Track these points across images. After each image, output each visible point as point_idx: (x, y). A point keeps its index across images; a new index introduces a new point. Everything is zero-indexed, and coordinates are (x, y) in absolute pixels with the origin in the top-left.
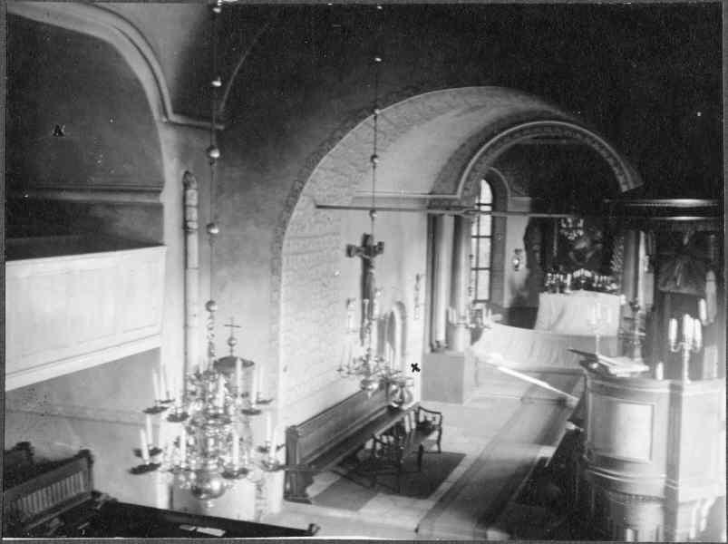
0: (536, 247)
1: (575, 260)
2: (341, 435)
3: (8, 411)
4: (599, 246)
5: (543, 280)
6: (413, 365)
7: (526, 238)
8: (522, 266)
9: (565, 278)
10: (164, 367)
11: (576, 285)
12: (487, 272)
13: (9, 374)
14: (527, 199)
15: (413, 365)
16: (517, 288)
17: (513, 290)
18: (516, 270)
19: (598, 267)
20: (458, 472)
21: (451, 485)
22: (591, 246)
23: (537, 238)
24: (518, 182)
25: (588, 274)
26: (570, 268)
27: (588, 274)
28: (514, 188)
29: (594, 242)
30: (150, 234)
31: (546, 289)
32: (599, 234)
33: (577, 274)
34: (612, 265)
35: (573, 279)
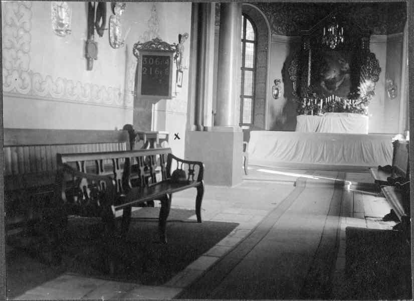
0: (293, 78)
1: (326, 88)
2: (143, 181)
3: (257, 99)
4: (347, 76)
5: (300, 105)
6: (175, 135)
7: (284, 72)
8: (281, 95)
9: (319, 101)
10: (2, 185)
11: (328, 108)
12: (250, 100)
13: (81, 151)
14: (285, 38)
15: (175, 135)
16: (276, 114)
17: (273, 114)
18: (276, 98)
19: (347, 93)
20: (224, 245)
21: (215, 259)
22: (340, 75)
23: (294, 70)
24: (278, 23)
25: (338, 99)
26: (322, 94)
27: (338, 99)
28: (274, 27)
29: (342, 73)
30: (262, 127)
31: (302, 113)
32: (347, 66)
33: (329, 99)
34: (359, 90)
35: (324, 104)
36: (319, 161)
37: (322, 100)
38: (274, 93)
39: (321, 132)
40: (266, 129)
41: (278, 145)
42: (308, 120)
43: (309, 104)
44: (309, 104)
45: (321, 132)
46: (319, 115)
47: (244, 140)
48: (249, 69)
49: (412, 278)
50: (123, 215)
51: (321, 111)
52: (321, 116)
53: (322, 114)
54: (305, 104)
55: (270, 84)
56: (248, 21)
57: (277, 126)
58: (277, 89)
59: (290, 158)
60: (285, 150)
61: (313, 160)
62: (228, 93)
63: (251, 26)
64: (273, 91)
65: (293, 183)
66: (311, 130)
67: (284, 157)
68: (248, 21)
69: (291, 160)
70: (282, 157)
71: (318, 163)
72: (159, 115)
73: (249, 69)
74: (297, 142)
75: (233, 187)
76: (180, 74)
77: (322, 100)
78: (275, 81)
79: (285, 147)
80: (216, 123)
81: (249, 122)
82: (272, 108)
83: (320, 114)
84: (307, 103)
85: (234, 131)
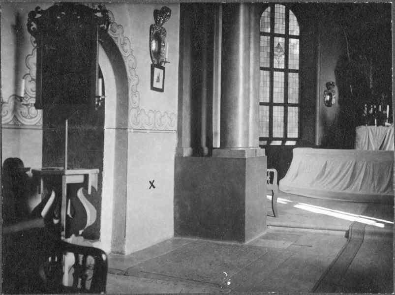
9: (384, 108)
36: (385, 191)
37: (388, 106)
38: (326, 100)
39: (387, 149)
40: (317, 144)
41: (328, 170)
42: (370, 133)
43: (371, 111)
44: (371, 111)
45: (387, 149)
46: (384, 125)
47: (269, 167)
48: (294, 71)
49: (393, 85)
50: (355, 130)
51: (387, 120)
52: (388, 126)
53: (389, 124)
54: (366, 112)
55: (321, 89)
56: (291, 12)
57: (327, 144)
58: (330, 95)
59: (345, 186)
60: (339, 174)
61: (376, 190)
62: (236, 99)
63: (295, 18)
64: (324, 98)
65: (345, 233)
66: (374, 147)
67: (337, 185)
68: (291, 12)
69: (345, 189)
70: (334, 183)
71: (385, 193)
72: (118, 137)
73: (294, 71)
74: (354, 162)
75: (247, 243)
76: (157, 70)
77: (388, 106)
78: (327, 84)
79: (338, 170)
80: (224, 143)
81: (296, 135)
82: (324, 117)
83: (387, 124)
84: (368, 111)
85: (246, 156)
